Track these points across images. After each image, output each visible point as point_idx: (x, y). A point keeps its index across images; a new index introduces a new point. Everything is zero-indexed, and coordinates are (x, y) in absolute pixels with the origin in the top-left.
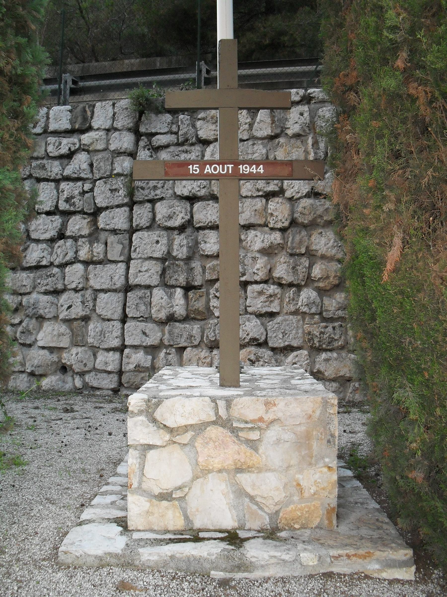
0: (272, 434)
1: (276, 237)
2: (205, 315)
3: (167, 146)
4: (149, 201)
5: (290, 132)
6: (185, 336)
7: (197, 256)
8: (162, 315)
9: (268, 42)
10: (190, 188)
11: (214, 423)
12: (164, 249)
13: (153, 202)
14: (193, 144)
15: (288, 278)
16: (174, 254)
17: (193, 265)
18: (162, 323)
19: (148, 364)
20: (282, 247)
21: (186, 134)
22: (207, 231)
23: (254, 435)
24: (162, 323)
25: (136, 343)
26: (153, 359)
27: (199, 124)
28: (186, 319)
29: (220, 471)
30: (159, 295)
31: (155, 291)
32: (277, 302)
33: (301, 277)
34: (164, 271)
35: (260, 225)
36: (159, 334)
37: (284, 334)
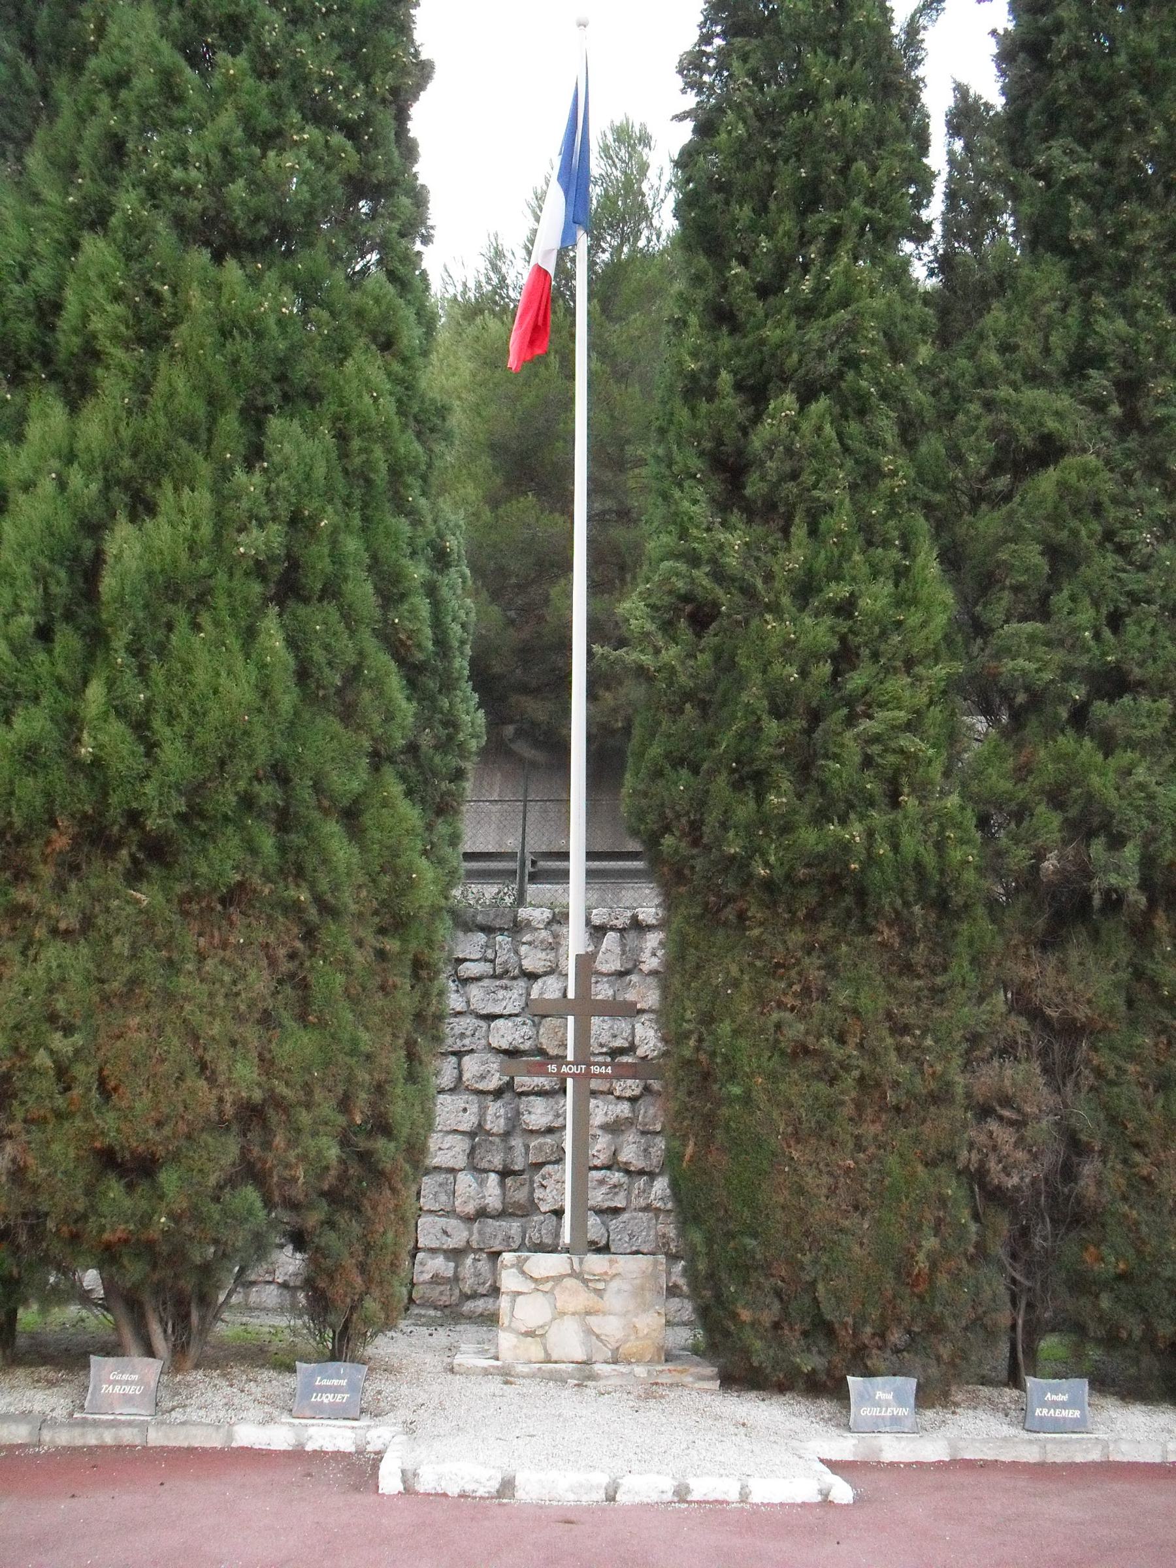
0: (614, 1285)
1: (624, 1109)
2: (527, 1209)
3: (478, 979)
4: (454, 1053)
5: (645, 968)
6: (500, 1237)
7: (518, 1130)
8: (470, 1208)
9: (620, 725)
10: (510, 1039)
11: (569, 1275)
12: (474, 1120)
13: (459, 1054)
14: (514, 978)
15: (638, 1163)
16: (488, 1127)
17: (513, 1143)
18: (469, 1219)
19: (450, 1273)
20: (630, 1122)
21: (506, 962)
22: (532, 1098)
23: (601, 1286)
24: (469, 1219)
25: (435, 1244)
26: (456, 1267)
27: (523, 949)
28: (502, 1214)
29: (573, 1314)
30: (465, 1180)
31: (460, 1176)
32: (623, 1194)
33: (655, 1162)
34: (473, 1149)
35: (602, 1093)
36: (465, 1234)
37: (631, 1236)
